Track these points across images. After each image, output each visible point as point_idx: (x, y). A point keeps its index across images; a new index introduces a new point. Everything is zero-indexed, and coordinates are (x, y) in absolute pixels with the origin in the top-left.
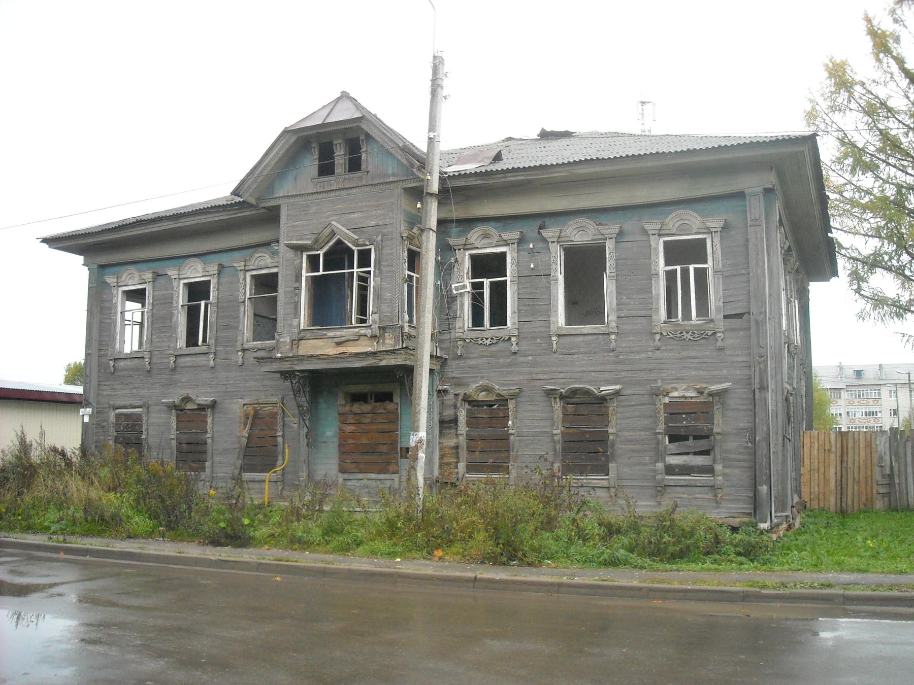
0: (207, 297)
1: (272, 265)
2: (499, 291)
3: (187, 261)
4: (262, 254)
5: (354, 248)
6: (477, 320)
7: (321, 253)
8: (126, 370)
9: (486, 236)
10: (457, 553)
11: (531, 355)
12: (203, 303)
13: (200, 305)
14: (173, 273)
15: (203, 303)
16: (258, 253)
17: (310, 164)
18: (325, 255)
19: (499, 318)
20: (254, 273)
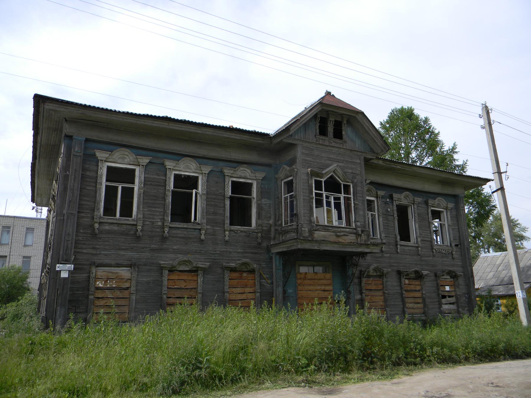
0: (196, 188)
1: (250, 178)
2: (128, 194)
3: (184, 159)
4: (245, 169)
5: (341, 182)
6: (109, 210)
7: (323, 180)
8: (468, 256)
9: (188, 167)
10: (351, 367)
11: (389, 253)
12: (194, 191)
13: (192, 193)
14: (227, 171)
15: (194, 191)
16: (242, 167)
17: (315, 128)
18: (324, 181)
19: (127, 211)
20: (234, 179)
